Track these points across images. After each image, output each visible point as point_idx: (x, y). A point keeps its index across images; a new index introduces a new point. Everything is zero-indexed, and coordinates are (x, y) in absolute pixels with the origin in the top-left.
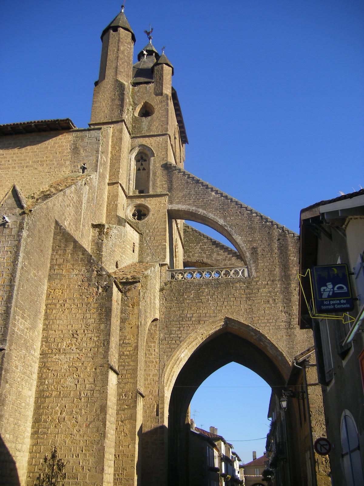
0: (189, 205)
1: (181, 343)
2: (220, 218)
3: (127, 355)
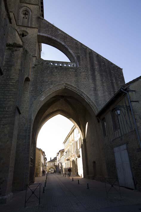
0: (48, 34)
1: (42, 92)
2: (63, 42)
3: (11, 85)
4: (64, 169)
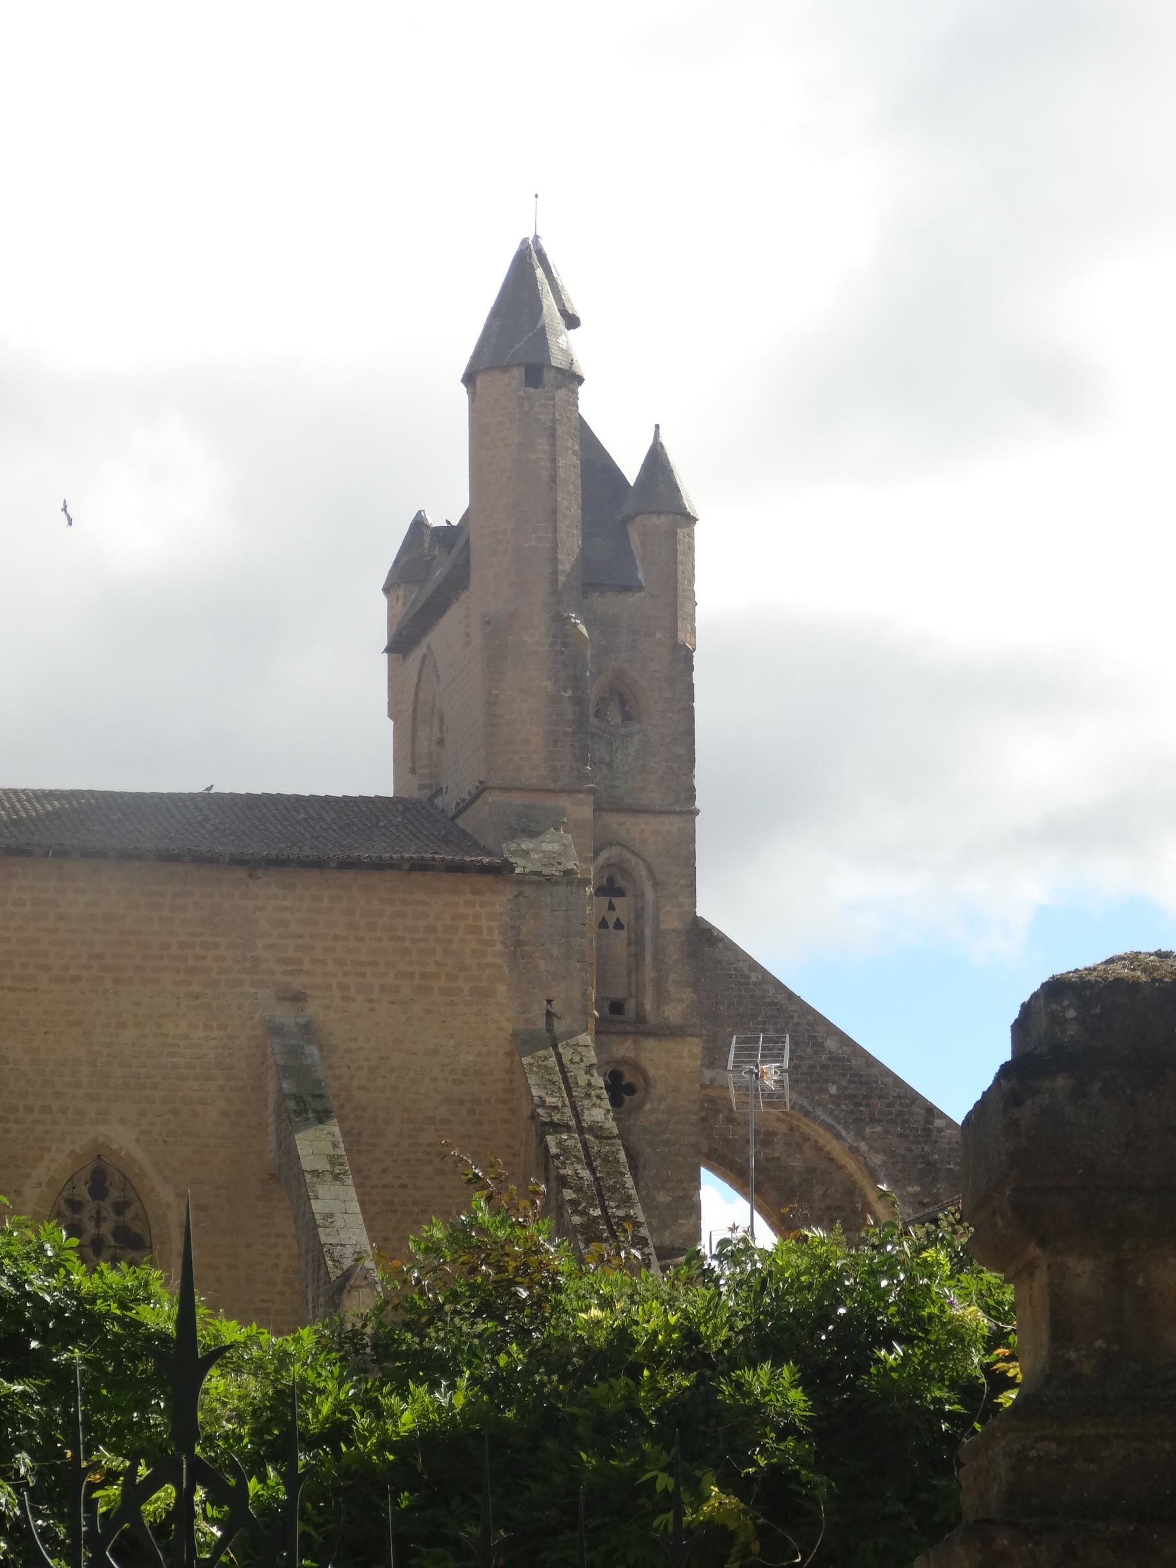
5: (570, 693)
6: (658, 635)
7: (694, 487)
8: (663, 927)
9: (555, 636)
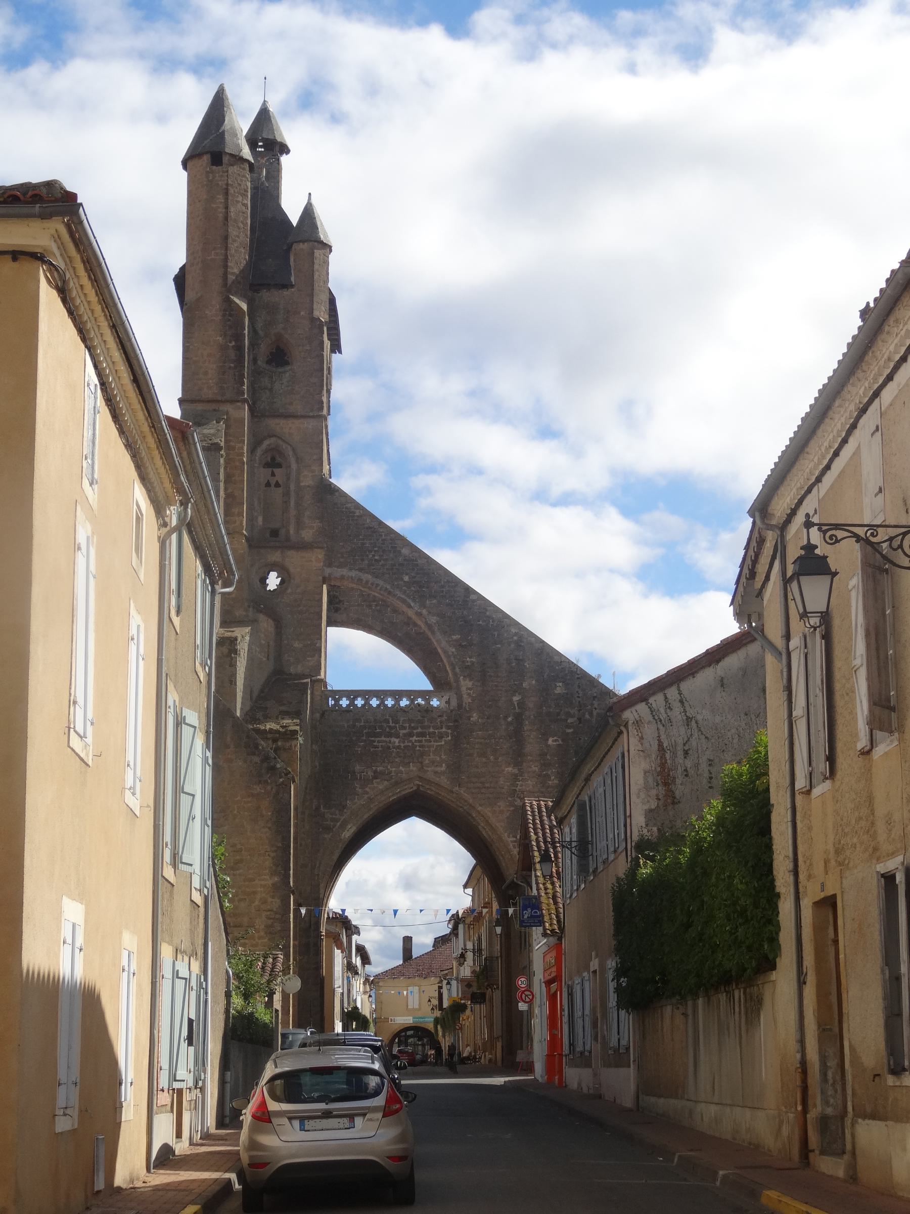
0: (361, 570)
4: (217, 1129)
5: (233, 343)
6: (302, 313)
7: (329, 226)
8: (302, 484)
9: (225, 310)
